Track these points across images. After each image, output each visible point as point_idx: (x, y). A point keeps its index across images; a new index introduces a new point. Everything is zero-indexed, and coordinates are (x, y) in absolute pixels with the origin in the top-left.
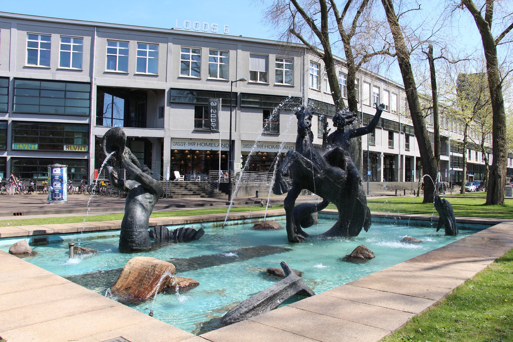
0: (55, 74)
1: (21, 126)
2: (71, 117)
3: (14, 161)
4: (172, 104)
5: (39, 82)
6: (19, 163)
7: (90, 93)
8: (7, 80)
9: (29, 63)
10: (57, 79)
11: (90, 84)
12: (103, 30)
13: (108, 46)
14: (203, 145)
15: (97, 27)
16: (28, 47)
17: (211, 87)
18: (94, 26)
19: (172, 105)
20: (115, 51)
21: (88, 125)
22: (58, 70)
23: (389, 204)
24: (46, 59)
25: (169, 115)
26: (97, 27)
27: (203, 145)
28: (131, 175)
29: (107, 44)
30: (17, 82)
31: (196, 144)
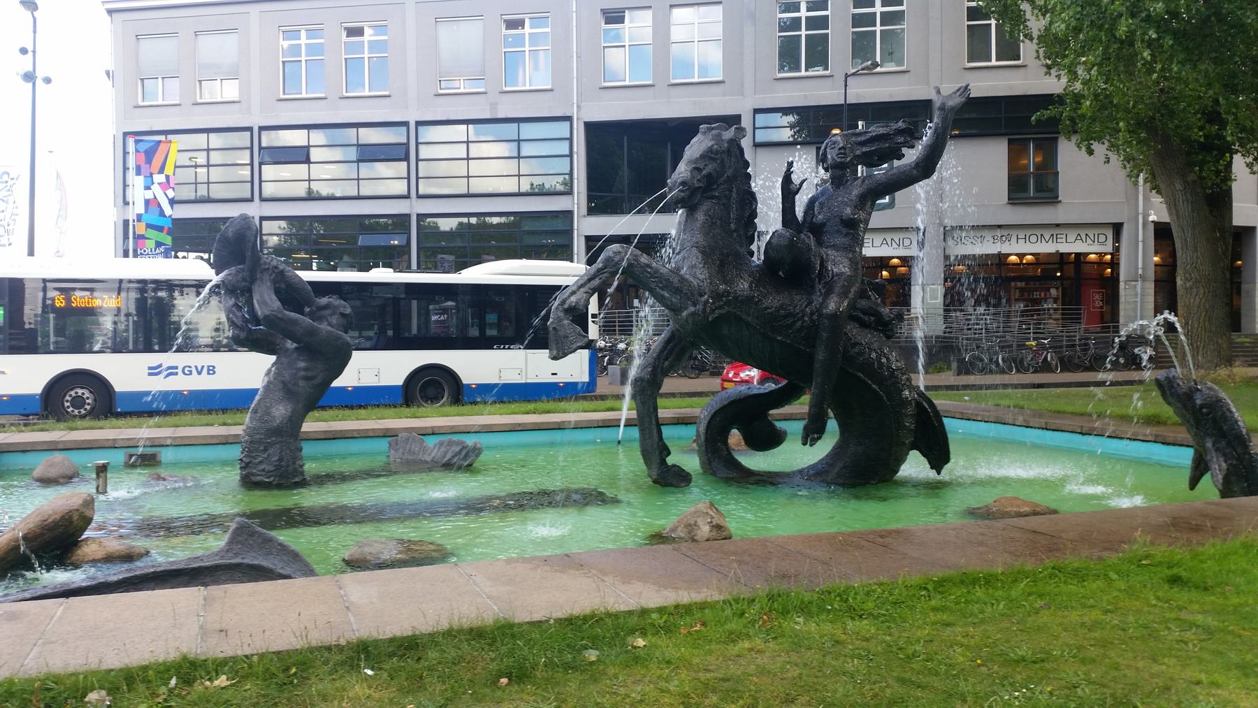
24: (818, 54)
31: (1014, 239)
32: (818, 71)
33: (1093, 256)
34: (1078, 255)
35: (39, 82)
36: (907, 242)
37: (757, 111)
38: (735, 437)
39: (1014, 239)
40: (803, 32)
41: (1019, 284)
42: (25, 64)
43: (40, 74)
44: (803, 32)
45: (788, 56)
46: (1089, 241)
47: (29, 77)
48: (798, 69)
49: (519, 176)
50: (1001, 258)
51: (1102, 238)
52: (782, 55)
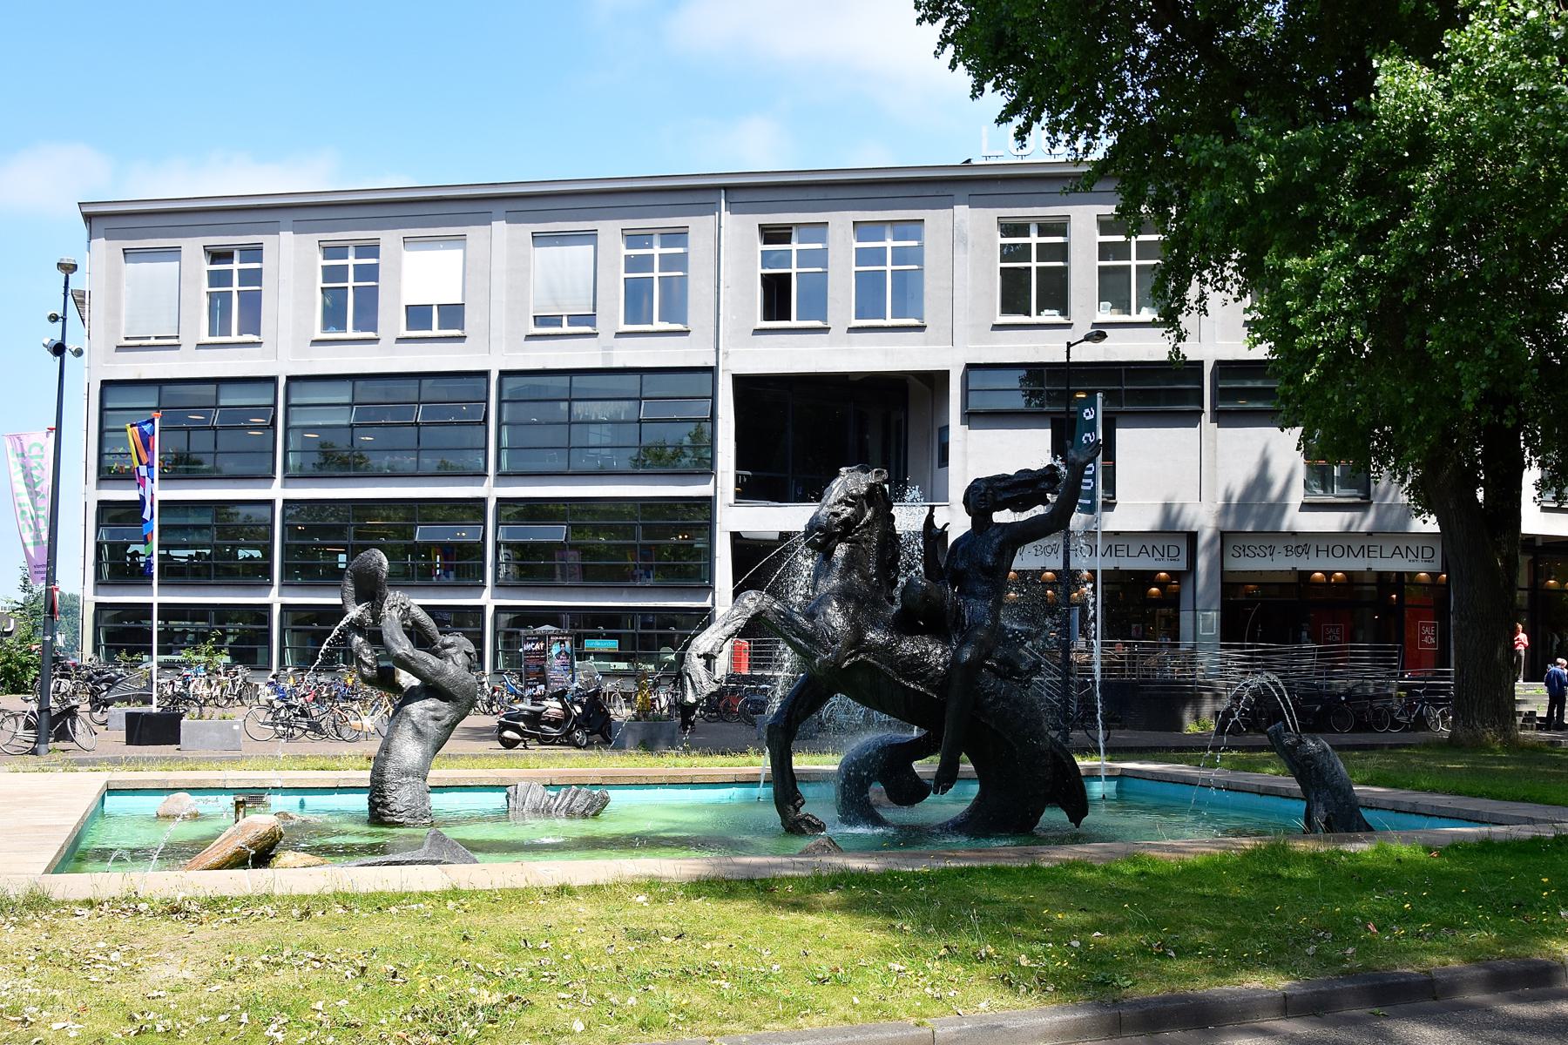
0: (612, 348)
1: (607, 514)
2: (230, 482)
3: (107, 614)
4: (973, 417)
5: (565, 380)
6: (118, 619)
7: (714, 397)
8: (271, 386)
9: (408, 329)
10: (615, 365)
11: (712, 370)
12: (742, 192)
13: (1102, 234)
14: (1338, 551)
15: (727, 188)
16: (763, 267)
17: (1037, 350)
18: (717, 188)
19: (973, 419)
20: (644, 263)
21: (707, 503)
22: (619, 335)
23: (1392, 814)
24: (1056, 293)
25: (965, 453)
26: (727, 188)
27: (1338, 551)
28: (405, 664)
29: (320, 256)
30: (510, 383)
31: (1313, 551)
32: (1051, 316)
33: (1049, 574)
34: (1400, 574)
35: (68, 354)
36: (1173, 552)
37: (970, 367)
38: (876, 791)
39: (1313, 551)
40: (656, 274)
41: (1165, 610)
42: (54, 333)
43: (70, 345)
44: (889, 268)
45: (1014, 295)
46: (1157, 555)
47: (59, 350)
48: (343, 327)
49: (570, 448)
50: (1305, 575)
51: (1173, 552)
52: (326, 311)
